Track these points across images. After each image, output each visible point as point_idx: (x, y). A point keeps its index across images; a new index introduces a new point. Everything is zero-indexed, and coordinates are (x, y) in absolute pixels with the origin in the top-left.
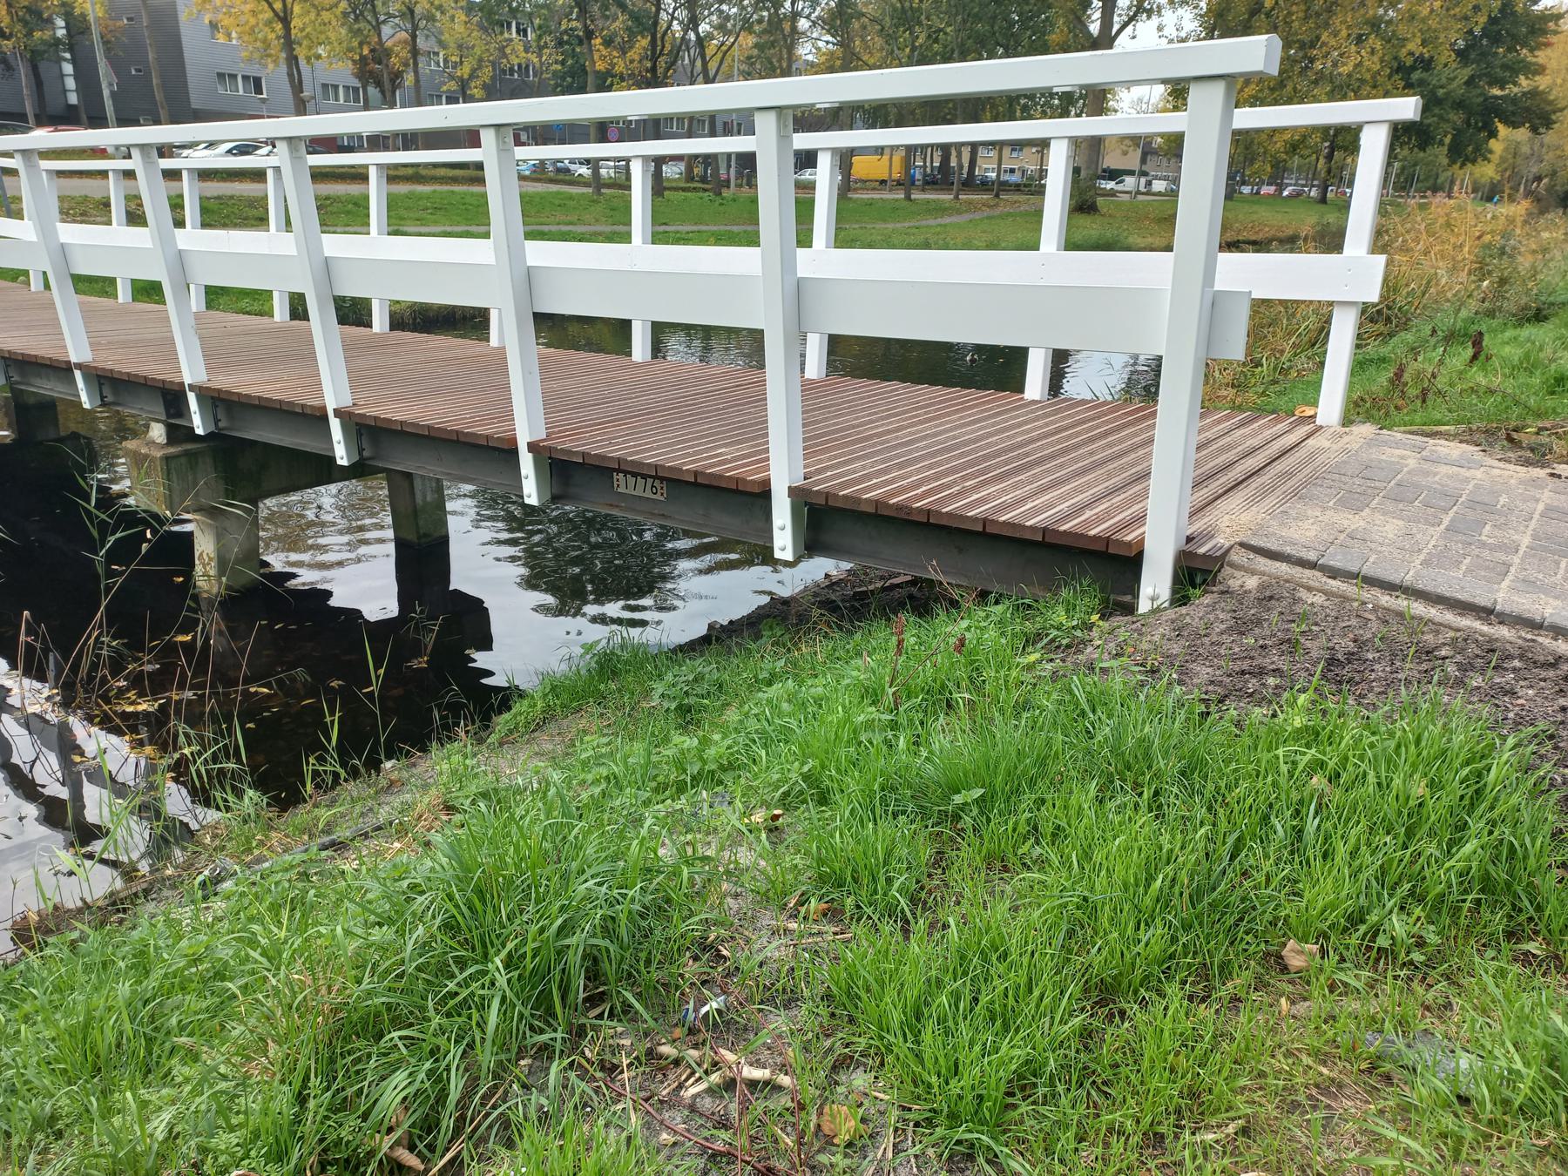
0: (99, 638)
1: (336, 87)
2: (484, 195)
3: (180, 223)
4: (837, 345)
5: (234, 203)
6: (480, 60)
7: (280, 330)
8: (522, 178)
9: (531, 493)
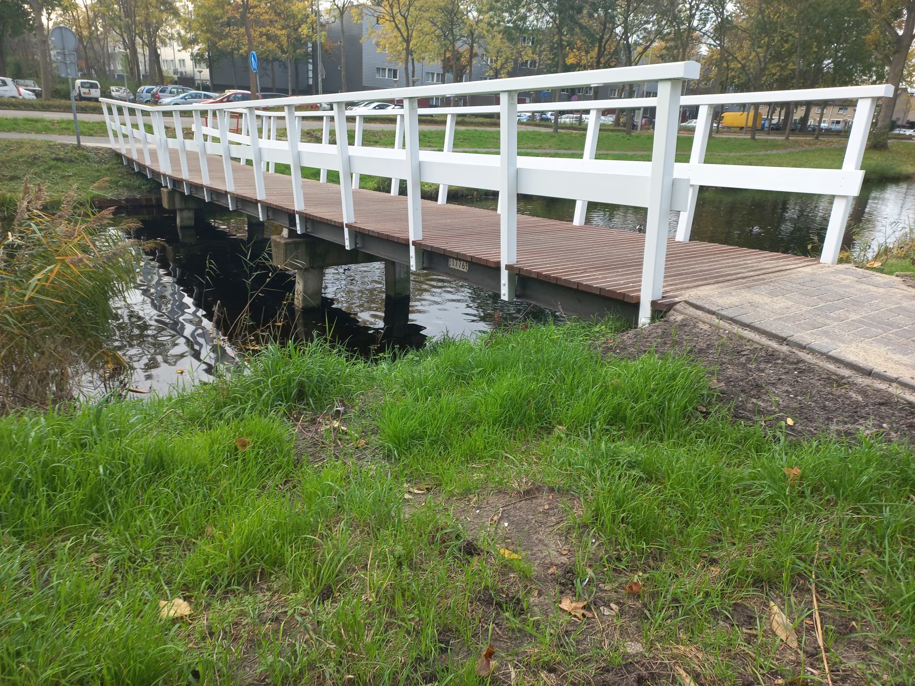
0: (245, 317)
1: (433, 74)
2: (499, 133)
3: (351, 143)
4: (363, 178)
5: (379, 133)
6: (507, 59)
7: (392, 200)
8: (520, 123)
9: (505, 293)
